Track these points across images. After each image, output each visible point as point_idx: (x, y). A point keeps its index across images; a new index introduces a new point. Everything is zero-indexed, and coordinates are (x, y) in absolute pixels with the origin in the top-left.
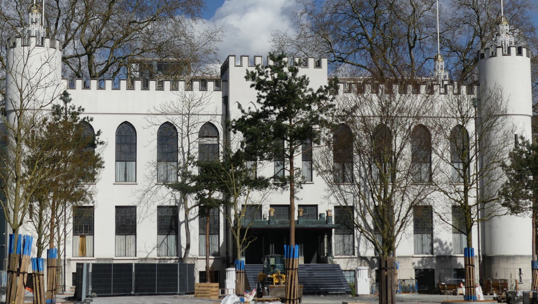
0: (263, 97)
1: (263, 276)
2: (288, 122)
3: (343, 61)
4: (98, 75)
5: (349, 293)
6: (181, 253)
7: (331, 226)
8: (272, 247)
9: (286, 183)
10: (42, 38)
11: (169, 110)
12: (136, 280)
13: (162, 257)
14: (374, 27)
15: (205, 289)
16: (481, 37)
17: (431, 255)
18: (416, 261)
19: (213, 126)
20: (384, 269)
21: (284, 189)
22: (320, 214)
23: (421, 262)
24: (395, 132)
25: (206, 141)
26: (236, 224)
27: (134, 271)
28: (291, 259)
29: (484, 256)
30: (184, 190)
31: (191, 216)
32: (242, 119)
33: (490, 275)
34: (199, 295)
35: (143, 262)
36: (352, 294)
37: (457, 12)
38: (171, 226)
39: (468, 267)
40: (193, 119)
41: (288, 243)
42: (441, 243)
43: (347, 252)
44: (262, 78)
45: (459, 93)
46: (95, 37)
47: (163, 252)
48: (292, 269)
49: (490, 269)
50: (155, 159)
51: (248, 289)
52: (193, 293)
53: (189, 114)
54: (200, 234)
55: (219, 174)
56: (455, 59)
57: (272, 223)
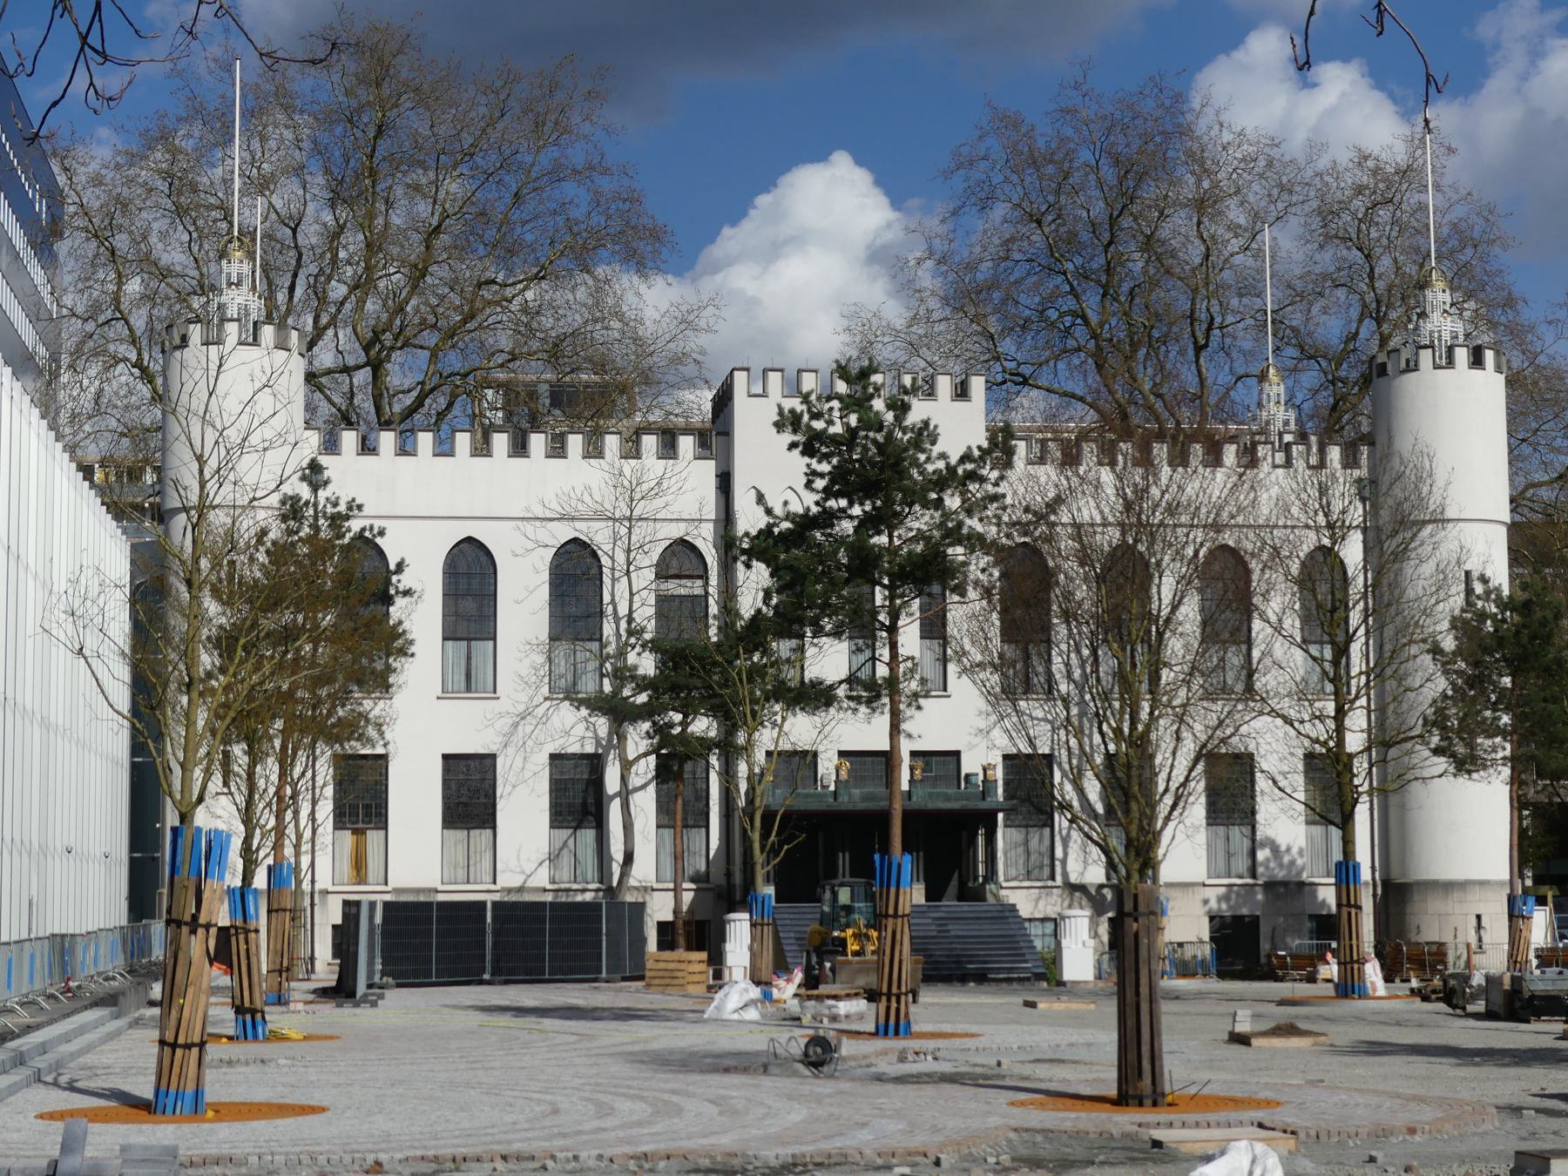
0: (822, 475)
1: (819, 933)
2: (883, 540)
3: (1025, 382)
4: (397, 419)
5: (1040, 977)
6: (611, 874)
7: (994, 806)
8: (843, 861)
9: (878, 696)
10: (255, 323)
11: (580, 507)
12: (495, 944)
13: (563, 886)
14: (1104, 295)
15: (671, 966)
16: (1379, 321)
17: (1250, 881)
18: (1212, 894)
19: (693, 548)
20: (1129, 915)
21: (874, 710)
22: (967, 776)
23: (1225, 898)
24: (1158, 564)
25: (674, 587)
26: (750, 801)
27: (489, 920)
28: (893, 890)
29: (1386, 883)
30: (619, 713)
31: (635, 781)
32: (767, 532)
33: (1402, 933)
34: (657, 981)
35: (514, 898)
36: (1047, 980)
37: (1317, 257)
38: (584, 804)
39: (1345, 910)
40: (640, 531)
41: (885, 849)
42: (1275, 850)
43: (1035, 873)
44: (819, 425)
45: (1322, 464)
46: (391, 322)
47: (565, 873)
48: (896, 916)
49: (1402, 916)
50: (544, 634)
51: (782, 966)
52: (642, 978)
53: (630, 519)
54: (658, 827)
55: (705, 676)
56: (1311, 377)
57: (843, 799)
